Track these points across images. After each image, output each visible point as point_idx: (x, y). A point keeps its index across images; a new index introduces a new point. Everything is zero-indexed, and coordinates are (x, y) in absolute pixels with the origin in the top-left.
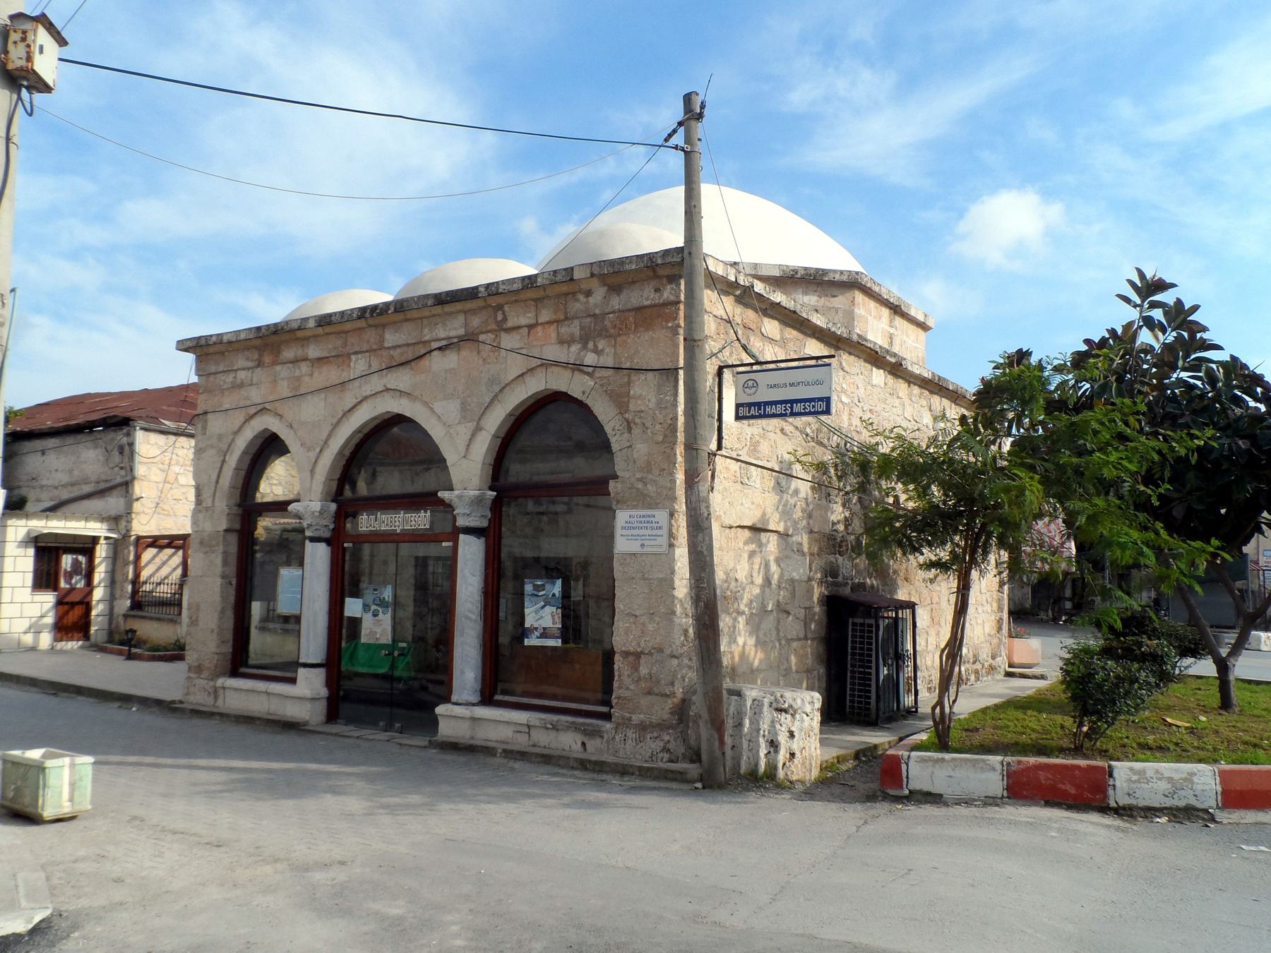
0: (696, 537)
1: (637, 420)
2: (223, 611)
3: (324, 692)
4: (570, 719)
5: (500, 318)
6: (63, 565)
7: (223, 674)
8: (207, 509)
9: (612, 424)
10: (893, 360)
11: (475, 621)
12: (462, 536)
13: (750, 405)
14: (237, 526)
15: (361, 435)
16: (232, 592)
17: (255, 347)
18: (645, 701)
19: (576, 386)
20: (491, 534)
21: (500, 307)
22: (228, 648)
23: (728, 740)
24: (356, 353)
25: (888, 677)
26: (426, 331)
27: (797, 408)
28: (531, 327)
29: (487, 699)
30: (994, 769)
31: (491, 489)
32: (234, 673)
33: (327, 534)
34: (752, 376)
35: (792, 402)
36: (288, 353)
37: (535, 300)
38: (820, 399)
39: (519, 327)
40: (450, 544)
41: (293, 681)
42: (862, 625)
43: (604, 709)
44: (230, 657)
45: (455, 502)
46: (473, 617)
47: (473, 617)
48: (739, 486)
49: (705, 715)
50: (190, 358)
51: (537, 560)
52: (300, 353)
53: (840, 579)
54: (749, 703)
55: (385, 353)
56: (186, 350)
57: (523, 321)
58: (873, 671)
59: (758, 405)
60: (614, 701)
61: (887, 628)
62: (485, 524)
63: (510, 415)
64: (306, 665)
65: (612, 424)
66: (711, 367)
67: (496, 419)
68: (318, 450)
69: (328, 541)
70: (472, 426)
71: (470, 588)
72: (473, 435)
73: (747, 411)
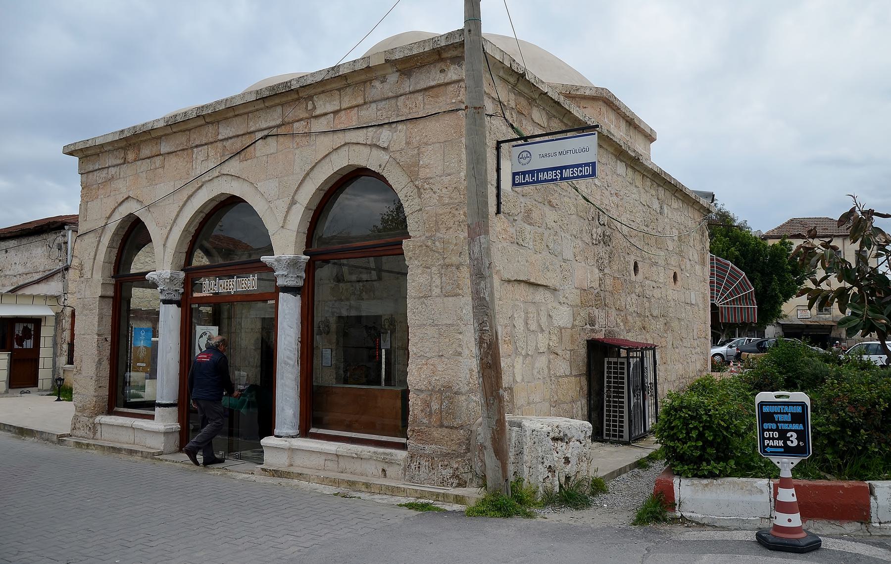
0: (479, 284)
1: (426, 186)
2: (100, 362)
3: (176, 426)
4: (372, 449)
5: (310, 107)
6: (17, 332)
7: (102, 413)
8: (87, 280)
9: (404, 191)
10: (633, 155)
11: (293, 366)
12: (281, 294)
13: (524, 173)
14: (111, 292)
15: (203, 215)
16: (107, 346)
17: (122, 148)
18: (436, 433)
19: (372, 160)
20: (306, 292)
21: (310, 98)
22: (105, 392)
23: (511, 468)
24: (197, 146)
25: (637, 405)
26: (251, 123)
27: (566, 173)
28: (335, 113)
29: (304, 433)
30: (762, 492)
31: (305, 253)
32: (110, 412)
33: (177, 297)
34: (526, 148)
35: (561, 168)
36: (146, 151)
37: (339, 90)
38: (587, 165)
39: (325, 114)
40: (273, 302)
41: (152, 417)
42: (615, 363)
43: (403, 440)
44: (106, 399)
45: (275, 265)
46: (291, 363)
47: (291, 363)
48: (515, 247)
49: (488, 444)
50: (75, 160)
51: (359, 318)
52: (155, 151)
53: (597, 327)
54: (528, 433)
55: (219, 144)
56: (71, 154)
57: (330, 108)
58: (625, 400)
59: (532, 172)
60: (409, 434)
61: (635, 365)
62: (300, 283)
63: (319, 189)
64: (160, 405)
65: (404, 191)
66: (491, 144)
67: (308, 193)
68: (168, 228)
69: (179, 304)
70: (288, 200)
71: (288, 338)
72: (289, 208)
73: (521, 178)
